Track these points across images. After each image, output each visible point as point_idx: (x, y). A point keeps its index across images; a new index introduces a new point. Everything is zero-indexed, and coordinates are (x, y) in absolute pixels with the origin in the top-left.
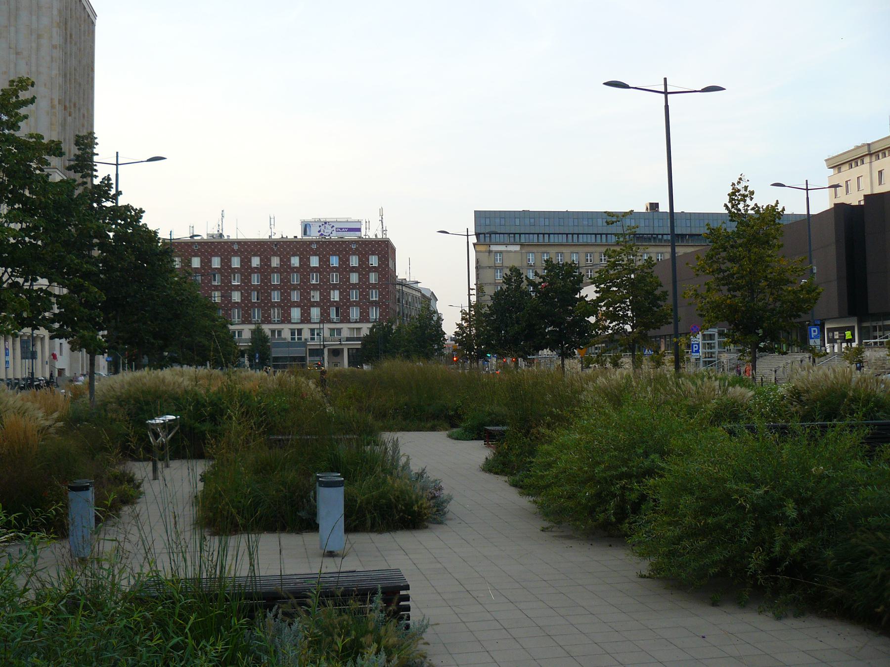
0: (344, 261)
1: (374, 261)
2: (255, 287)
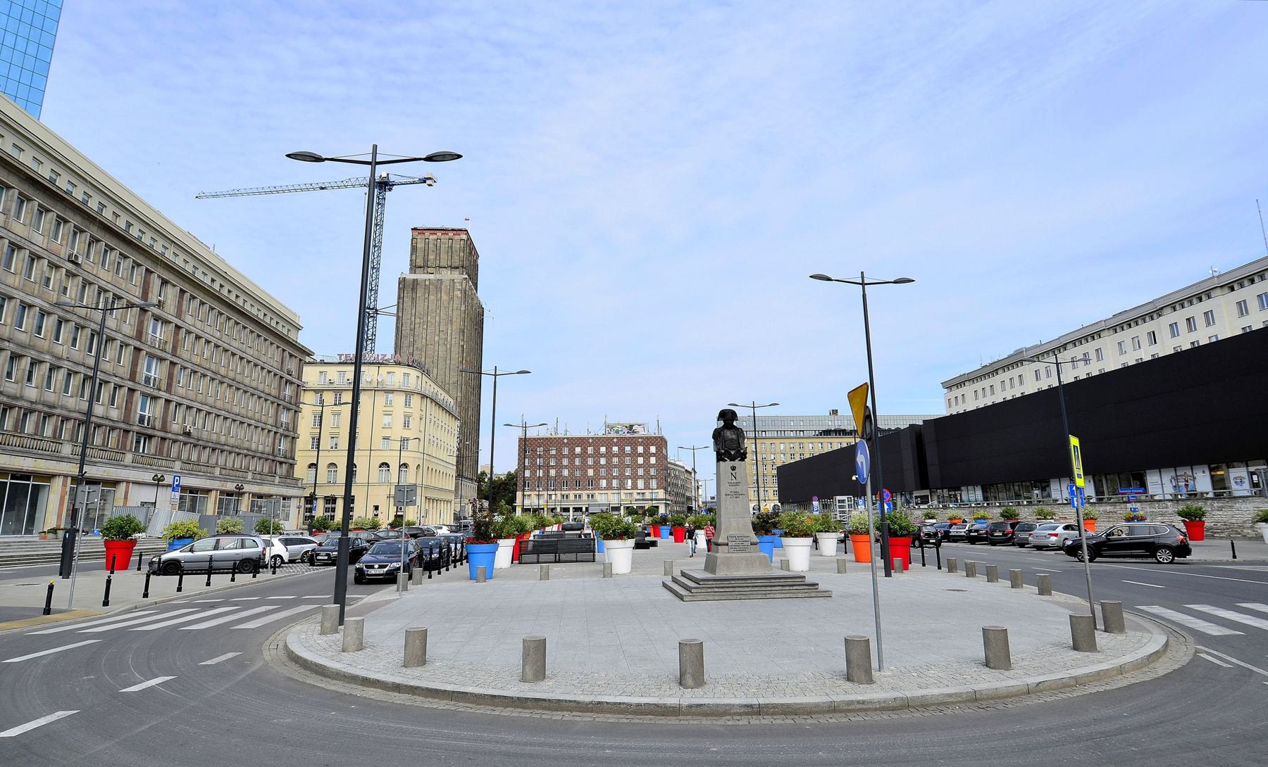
0: (634, 450)
1: (653, 449)
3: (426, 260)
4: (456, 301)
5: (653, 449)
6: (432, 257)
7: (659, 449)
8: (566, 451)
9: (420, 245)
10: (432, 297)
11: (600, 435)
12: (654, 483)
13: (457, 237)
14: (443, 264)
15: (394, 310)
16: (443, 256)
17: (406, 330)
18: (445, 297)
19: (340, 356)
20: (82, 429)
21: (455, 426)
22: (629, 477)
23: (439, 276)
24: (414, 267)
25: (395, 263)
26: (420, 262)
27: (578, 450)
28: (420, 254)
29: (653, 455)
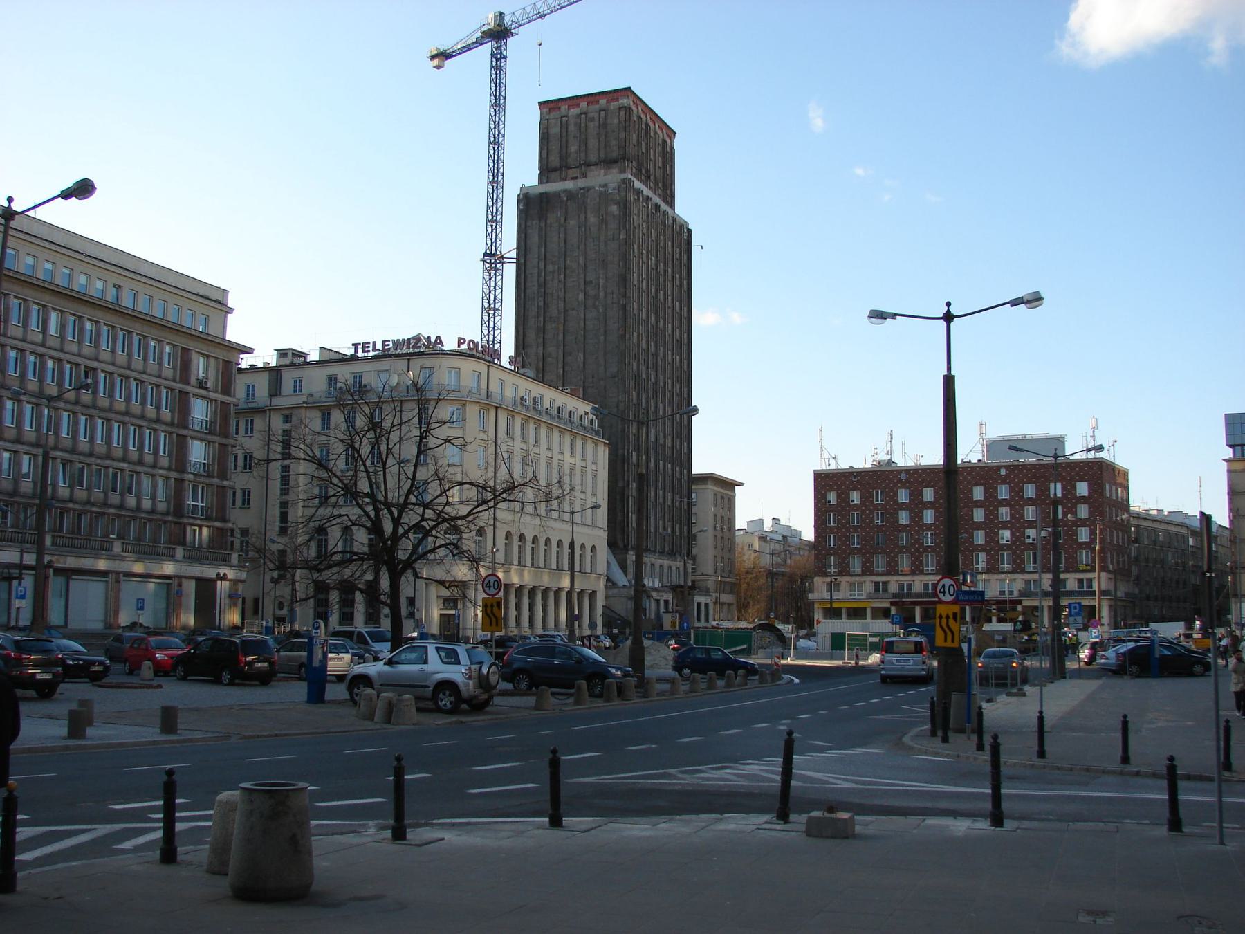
1: (1082, 489)
2: (929, 527)
3: (564, 155)
4: (613, 225)
5: (1082, 489)
6: (573, 148)
7: (1096, 488)
8: (1004, 492)
9: (555, 130)
10: (572, 223)
11: (974, 461)
12: (930, 564)
13: (613, 105)
14: (593, 158)
15: (514, 254)
16: (593, 143)
17: (533, 289)
18: (592, 220)
19: (356, 345)
20: (562, 229)
21: (603, 454)
22: (982, 548)
23: (581, 183)
24: (546, 170)
25: (523, 169)
26: (555, 161)
27: (1030, 491)
28: (555, 146)
29: (1083, 500)
